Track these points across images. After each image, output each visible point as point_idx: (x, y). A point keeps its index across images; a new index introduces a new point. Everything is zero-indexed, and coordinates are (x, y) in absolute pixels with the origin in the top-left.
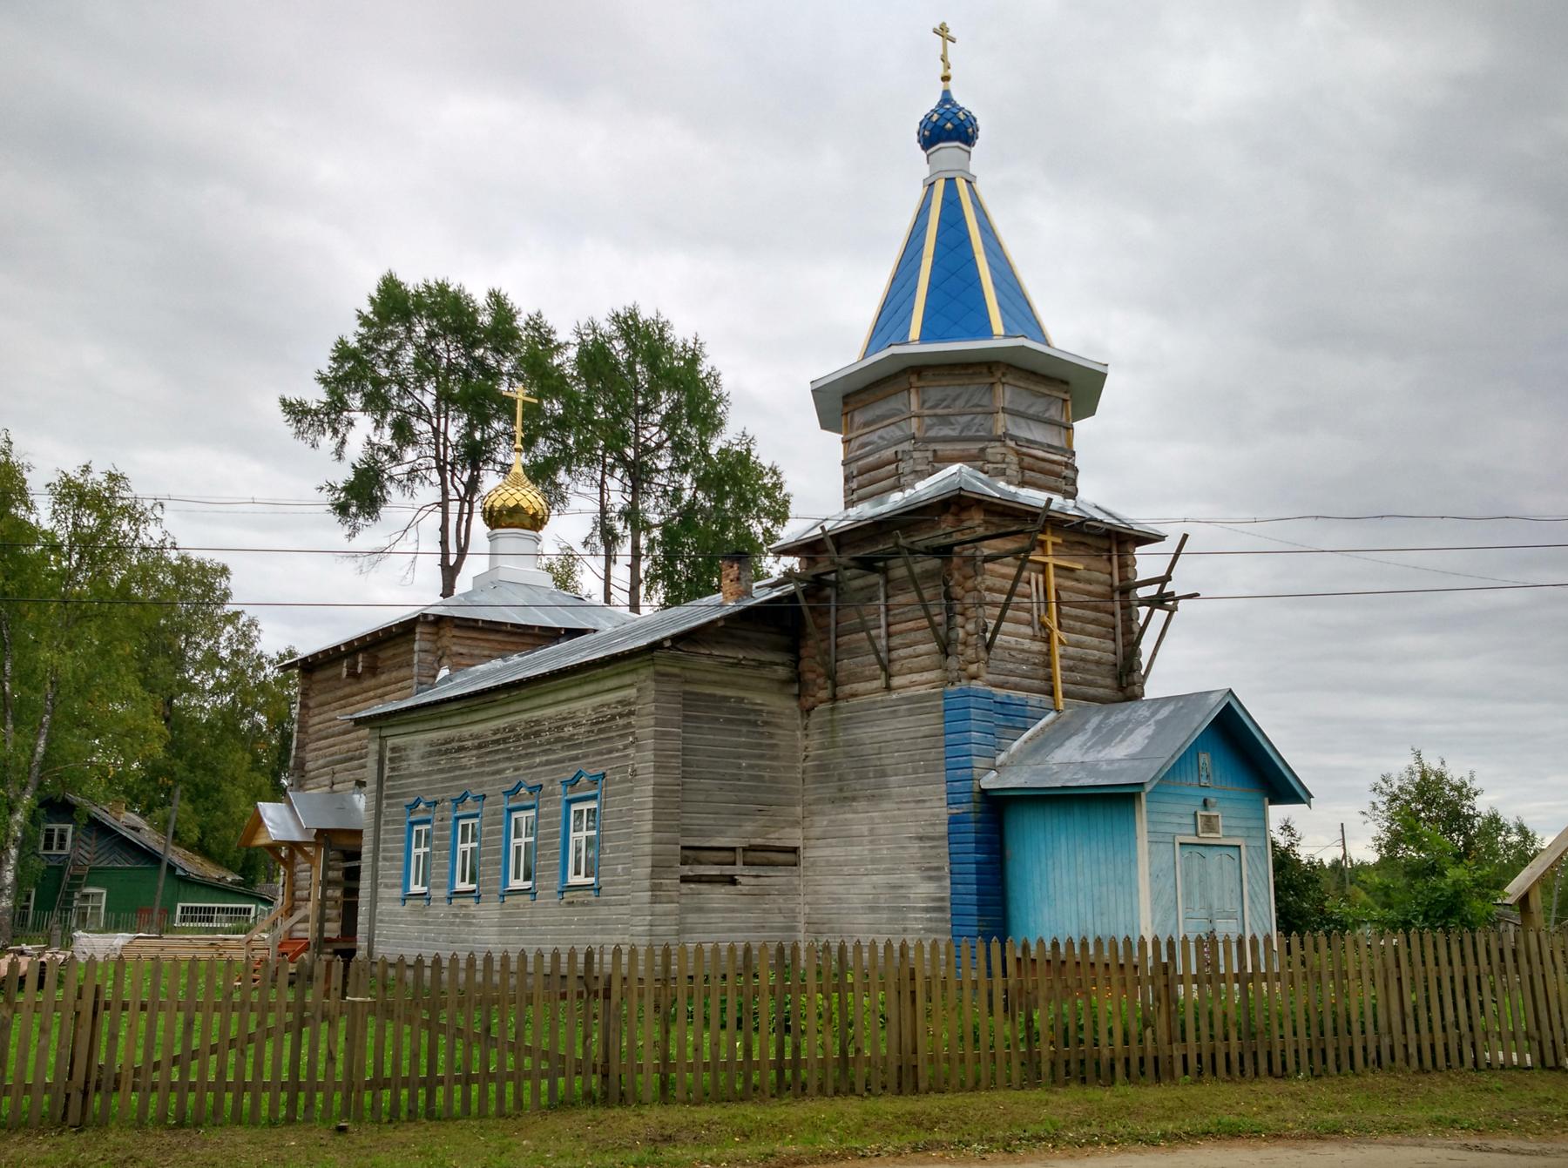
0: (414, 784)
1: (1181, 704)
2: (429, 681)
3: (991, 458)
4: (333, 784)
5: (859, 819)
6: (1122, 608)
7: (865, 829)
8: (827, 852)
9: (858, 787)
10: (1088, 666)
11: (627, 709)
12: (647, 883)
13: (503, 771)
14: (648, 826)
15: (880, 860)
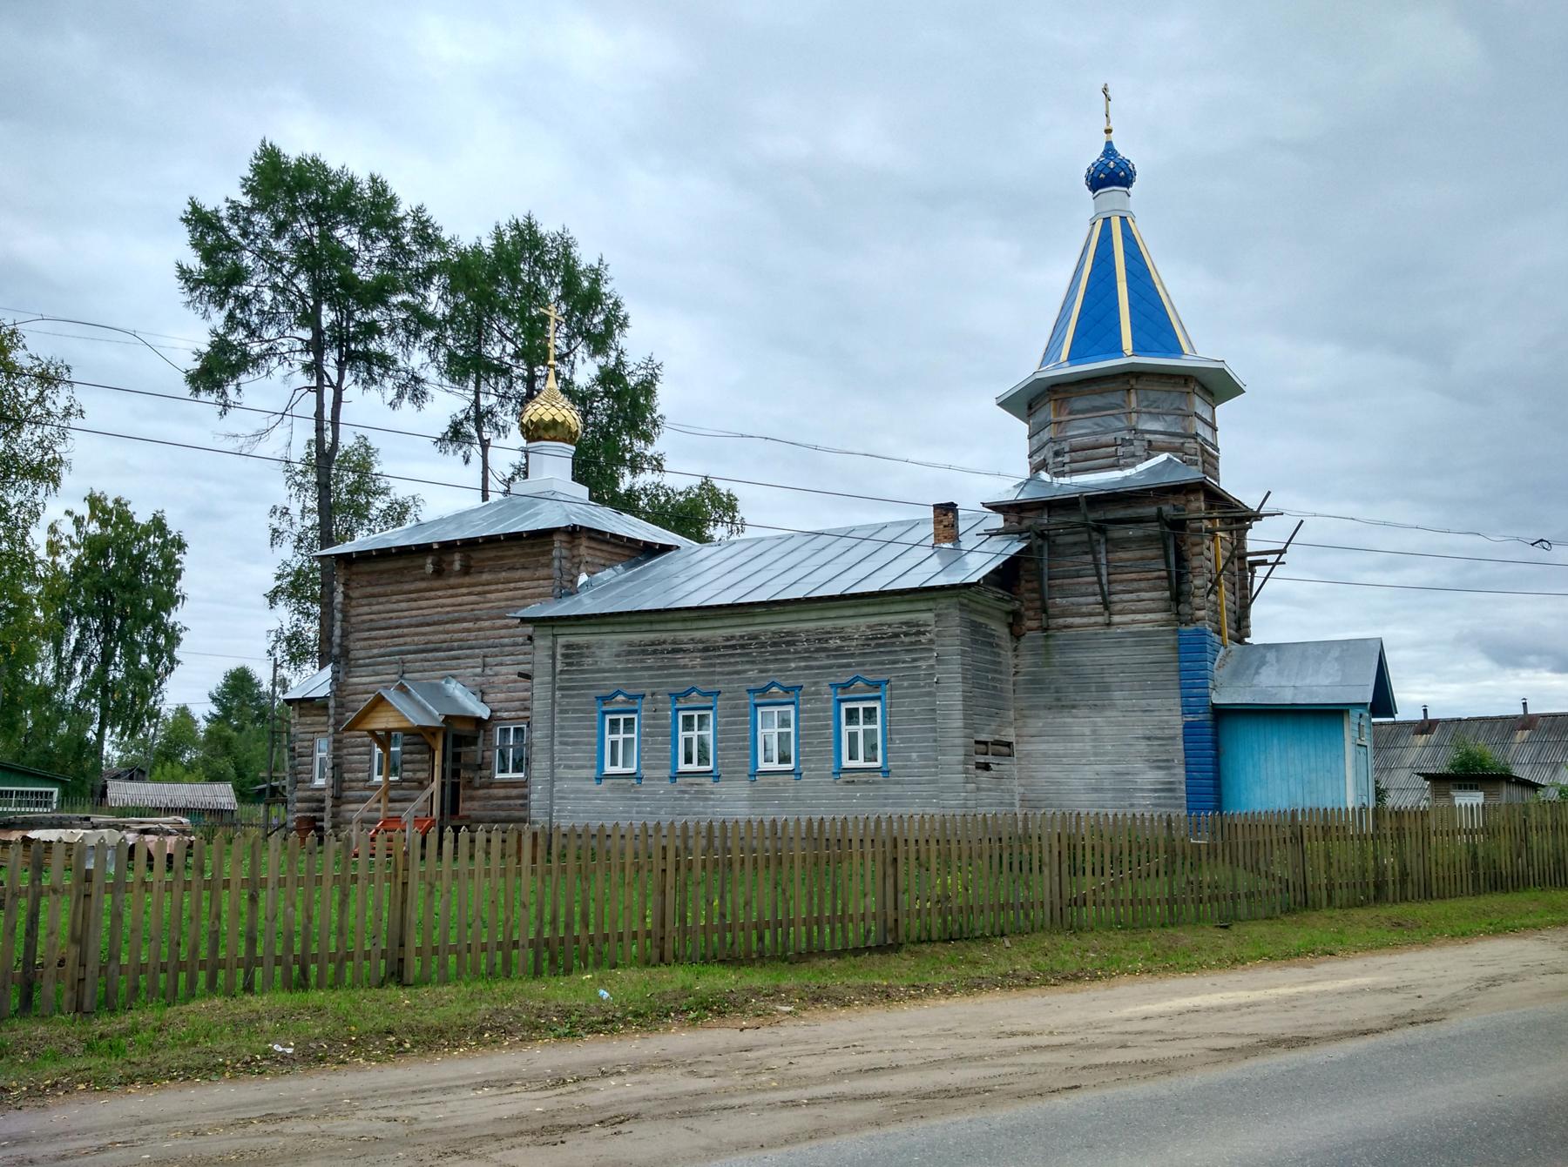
0: (605, 679)
1: (1345, 647)
2: (568, 589)
3: (1187, 451)
4: (403, 673)
5: (1080, 723)
6: (1239, 570)
7: (1087, 731)
8: (1044, 746)
9: (1078, 698)
11: (914, 630)
12: (960, 768)
13: (745, 671)
14: (960, 724)
15: (1105, 754)
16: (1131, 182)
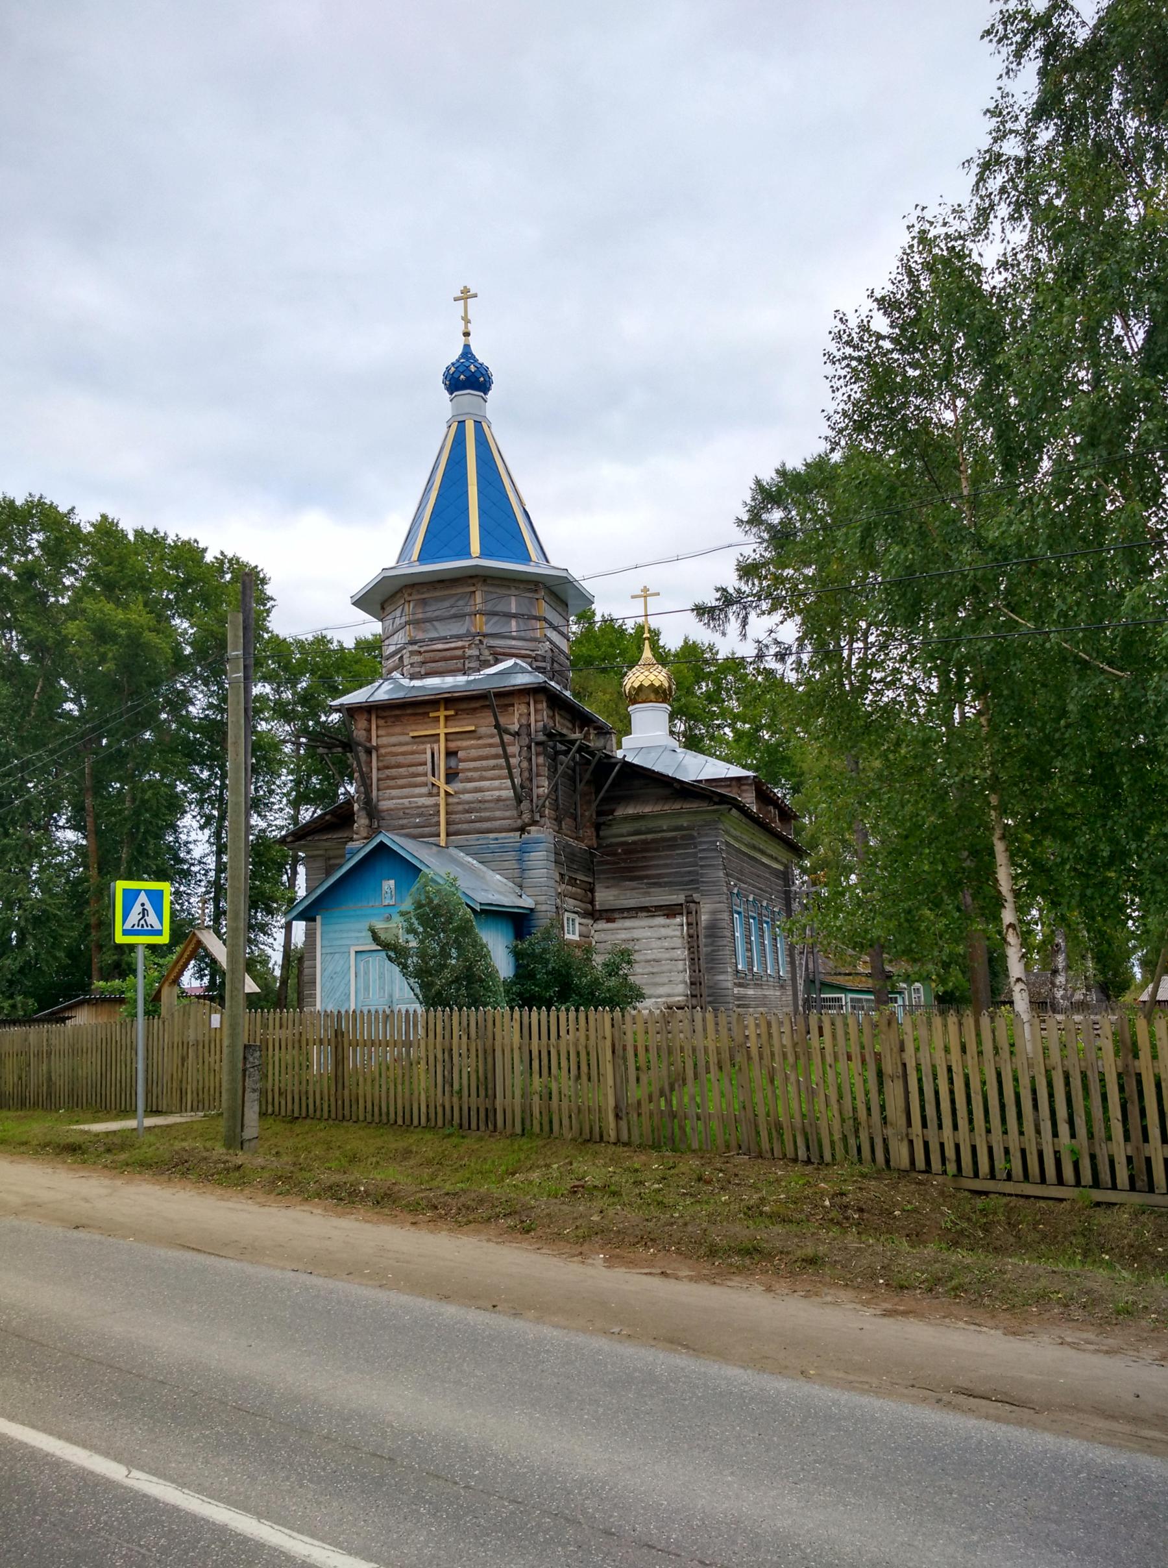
10: (487, 805)
16: (489, 389)
